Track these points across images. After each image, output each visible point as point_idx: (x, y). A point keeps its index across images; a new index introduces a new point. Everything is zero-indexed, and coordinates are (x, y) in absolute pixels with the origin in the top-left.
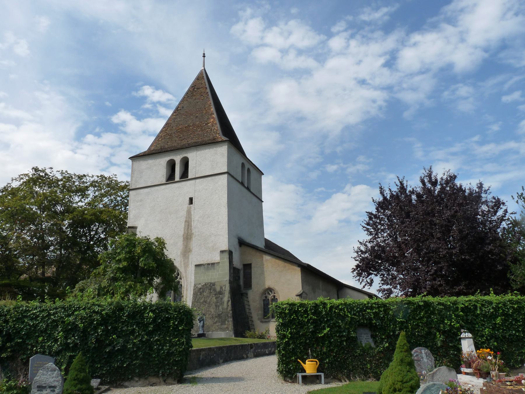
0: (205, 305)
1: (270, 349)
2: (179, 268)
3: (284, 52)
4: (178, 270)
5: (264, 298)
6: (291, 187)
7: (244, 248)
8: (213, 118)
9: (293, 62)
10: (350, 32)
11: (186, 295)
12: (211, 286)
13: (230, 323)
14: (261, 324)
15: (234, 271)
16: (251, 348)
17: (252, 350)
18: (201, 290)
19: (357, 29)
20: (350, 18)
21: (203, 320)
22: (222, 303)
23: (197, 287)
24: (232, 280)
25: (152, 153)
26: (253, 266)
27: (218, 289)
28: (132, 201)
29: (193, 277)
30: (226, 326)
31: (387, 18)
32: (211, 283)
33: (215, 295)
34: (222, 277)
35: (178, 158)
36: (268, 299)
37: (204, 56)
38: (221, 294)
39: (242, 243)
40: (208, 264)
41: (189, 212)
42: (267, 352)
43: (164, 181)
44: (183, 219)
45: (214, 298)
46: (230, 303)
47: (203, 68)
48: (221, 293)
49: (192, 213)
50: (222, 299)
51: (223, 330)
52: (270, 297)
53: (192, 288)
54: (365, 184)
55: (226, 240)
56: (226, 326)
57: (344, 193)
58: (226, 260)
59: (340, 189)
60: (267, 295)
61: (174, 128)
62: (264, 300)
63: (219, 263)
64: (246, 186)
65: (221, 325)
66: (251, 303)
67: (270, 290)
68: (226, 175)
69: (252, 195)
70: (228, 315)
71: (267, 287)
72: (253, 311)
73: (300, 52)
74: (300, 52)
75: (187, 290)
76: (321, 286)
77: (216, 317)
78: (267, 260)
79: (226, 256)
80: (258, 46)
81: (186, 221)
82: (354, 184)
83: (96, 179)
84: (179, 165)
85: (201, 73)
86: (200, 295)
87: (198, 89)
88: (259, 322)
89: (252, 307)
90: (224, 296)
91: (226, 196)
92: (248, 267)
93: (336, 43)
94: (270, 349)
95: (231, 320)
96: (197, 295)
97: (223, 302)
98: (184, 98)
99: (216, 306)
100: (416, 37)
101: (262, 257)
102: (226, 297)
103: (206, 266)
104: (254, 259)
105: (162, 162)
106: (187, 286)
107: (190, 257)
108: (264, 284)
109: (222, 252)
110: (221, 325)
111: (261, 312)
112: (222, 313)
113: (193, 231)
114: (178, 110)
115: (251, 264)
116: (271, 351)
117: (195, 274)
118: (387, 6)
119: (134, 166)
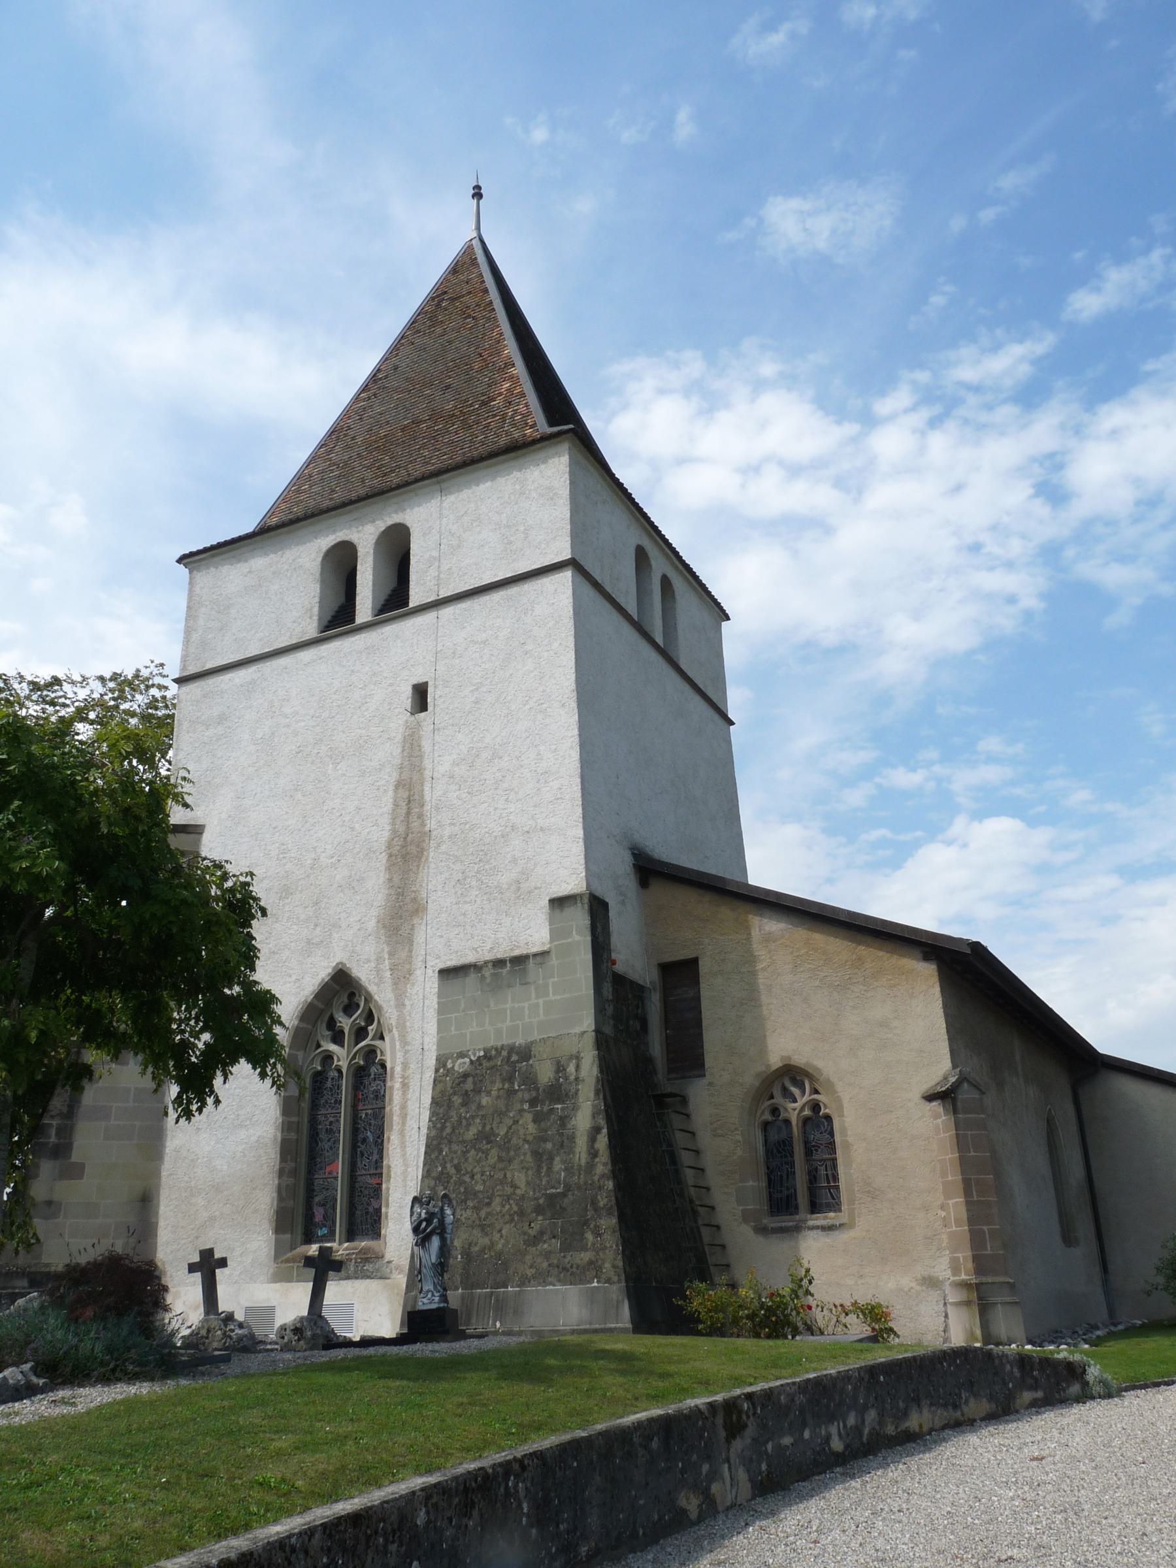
0: (486, 1153)
1: (851, 1420)
2: (372, 989)
3: (751, 470)
4: (369, 998)
5: (767, 1117)
6: (792, 831)
7: (661, 892)
8: (512, 377)
9: (775, 496)
10: (925, 414)
11: (404, 1107)
12: (507, 1065)
13: (605, 1240)
14: (761, 1239)
15: (617, 995)
16: (734, 1429)
17: (738, 1445)
18: (469, 1085)
19: (941, 405)
20: (923, 376)
21: (441, 1231)
22: (566, 1142)
23: (449, 1072)
24: (608, 1030)
25: (274, 530)
26: (704, 967)
27: (545, 1074)
28: (185, 725)
29: (432, 1027)
30: (586, 1256)
31: (1025, 369)
32: (512, 1049)
33: (533, 1102)
34: (561, 1017)
35: (364, 536)
36: (787, 1122)
37: (478, 194)
38: (559, 1100)
39: (649, 871)
40: (499, 963)
41: (412, 746)
42: (837, 1445)
43: (311, 629)
44: (388, 778)
45: (528, 1117)
46: (602, 1141)
47: (475, 234)
48: (558, 1092)
49: (426, 745)
50: (564, 1120)
51: (572, 1275)
52: (795, 1109)
53: (429, 1075)
54: (1007, 814)
55: (577, 850)
56: (586, 1256)
57: (949, 843)
58: (577, 938)
59: (934, 832)
60: (779, 1100)
61: (359, 440)
62: (766, 1126)
63: (544, 954)
64: (659, 640)
65: (566, 1248)
66: (705, 1139)
67: (793, 1075)
68: (567, 575)
69: (687, 688)
70: (594, 1202)
71: (775, 1060)
72: (713, 1178)
73: (794, 470)
74: (794, 470)
75: (405, 1086)
76: (1018, 1057)
77: (539, 1210)
78: (768, 939)
79: (580, 918)
80: (682, 461)
81: (399, 785)
82: (979, 815)
83: (97, 689)
84: (370, 559)
85: (468, 250)
86: (464, 1104)
87: (453, 300)
88: (747, 1230)
89: (709, 1160)
90: (575, 1108)
91: (569, 658)
92: (681, 974)
93: (890, 443)
94: (851, 1420)
95: (609, 1223)
96: (450, 1105)
97: (572, 1138)
98: (403, 336)
99: (537, 1155)
100: (1114, 415)
101: (747, 929)
102: (585, 1114)
103: (487, 972)
104: (705, 934)
105: (306, 556)
106: (405, 1066)
107: (419, 937)
108: (763, 1051)
109: (558, 903)
110: (566, 1248)
111: (755, 1184)
112: (568, 1188)
113: (431, 824)
114: (375, 382)
115: (695, 961)
116: (858, 1429)
117: (442, 1009)
118: (1021, 341)
119: (197, 589)
